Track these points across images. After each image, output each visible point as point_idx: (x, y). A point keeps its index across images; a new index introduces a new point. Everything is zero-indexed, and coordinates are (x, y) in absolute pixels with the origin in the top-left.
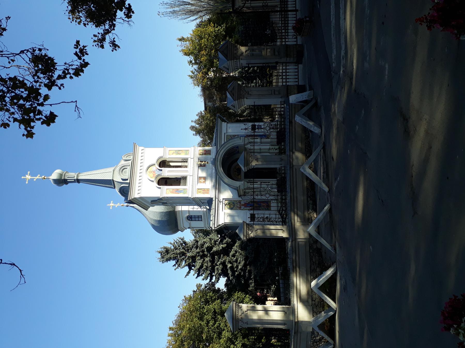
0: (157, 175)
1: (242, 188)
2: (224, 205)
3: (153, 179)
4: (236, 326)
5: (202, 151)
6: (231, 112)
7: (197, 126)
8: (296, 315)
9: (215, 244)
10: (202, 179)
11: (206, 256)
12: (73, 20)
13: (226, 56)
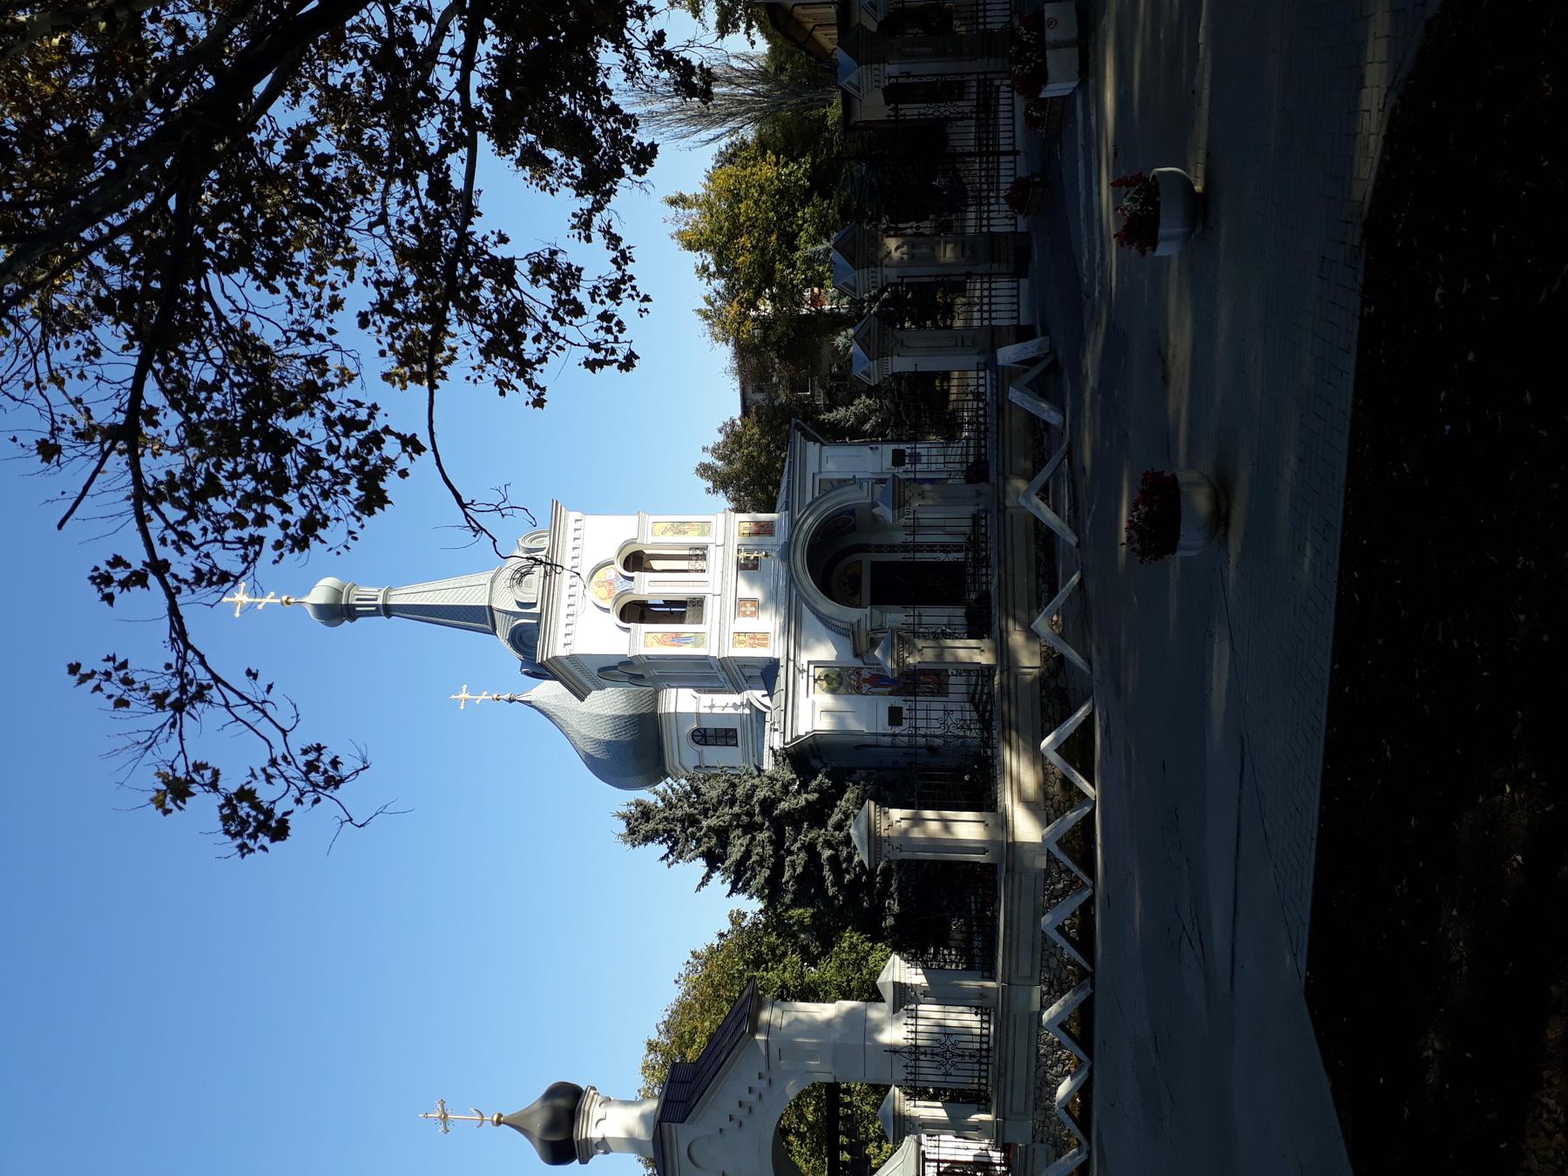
1: (866, 625)
2: (811, 679)
3: (608, 604)
5: (747, 525)
7: (719, 463)
8: (1011, 830)
9: (787, 793)
10: (748, 605)
11: (760, 828)
13: (851, 259)
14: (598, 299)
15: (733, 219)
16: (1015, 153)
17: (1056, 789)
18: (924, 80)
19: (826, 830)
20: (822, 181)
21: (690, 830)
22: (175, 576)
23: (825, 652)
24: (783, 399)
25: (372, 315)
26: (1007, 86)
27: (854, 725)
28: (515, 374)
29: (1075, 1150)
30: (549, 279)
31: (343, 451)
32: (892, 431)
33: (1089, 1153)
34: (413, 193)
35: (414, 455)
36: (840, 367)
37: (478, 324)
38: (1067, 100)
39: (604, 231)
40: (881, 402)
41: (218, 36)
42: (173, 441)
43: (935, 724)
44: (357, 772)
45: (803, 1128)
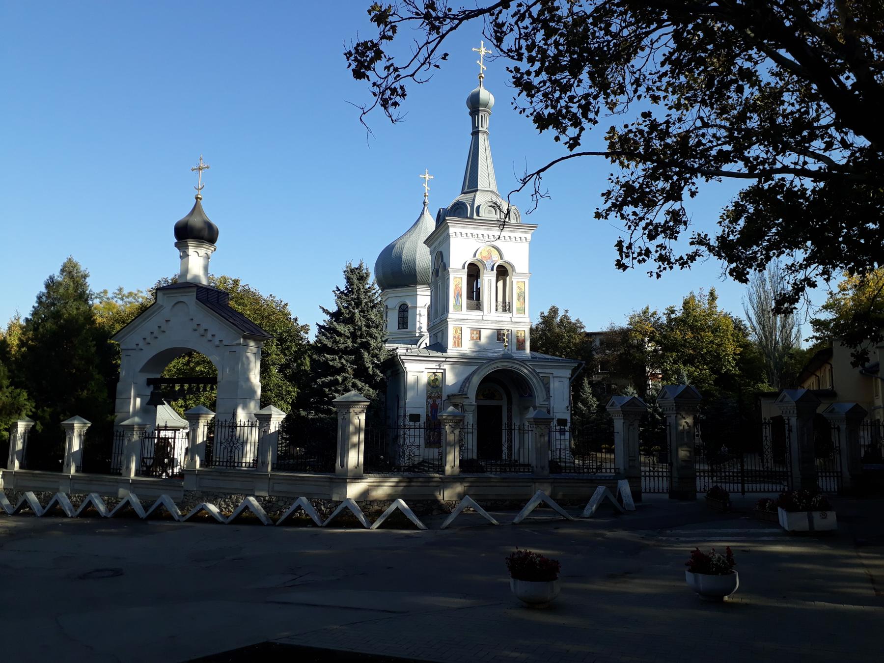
0: (485, 262)
1: (466, 402)
2: (435, 371)
6: (584, 380)
7: (558, 320)
9: (373, 357)
11: (354, 342)
12: (725, 210)
13: (680, 396)
14: (658, 249)
15: (702, 328)
16: (743, 492)
17: (376, 507)
18: (787, 440)
19: (352, 378)
20: (725, 380)
21: (353, 303)
22: (500, 12)
23: (450, 379)
24: (596, 356)
25: (649, 120)
26: (784, 489)
27: (410, 395)
28: (615, 201)
29: (180, 513)
30: (670, 221)
31: (571, 104)
32: (578, 419)
33: (179, 521)
34: (720, 142)
35: (568, 144)
36: (615, 389)
37: (643, 180)
38: (776, 523)
39: (697, 252)
40: (594, 413)
41: (814, 29)
42: (576, 9)
43: (412, 440)
44: (390, 117)
45: (192, 365)
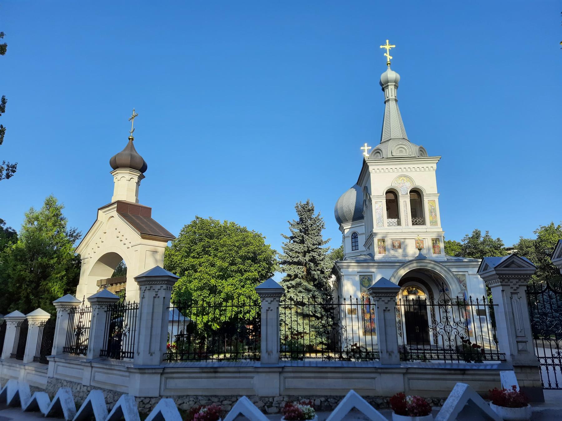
4: (157, 281)
